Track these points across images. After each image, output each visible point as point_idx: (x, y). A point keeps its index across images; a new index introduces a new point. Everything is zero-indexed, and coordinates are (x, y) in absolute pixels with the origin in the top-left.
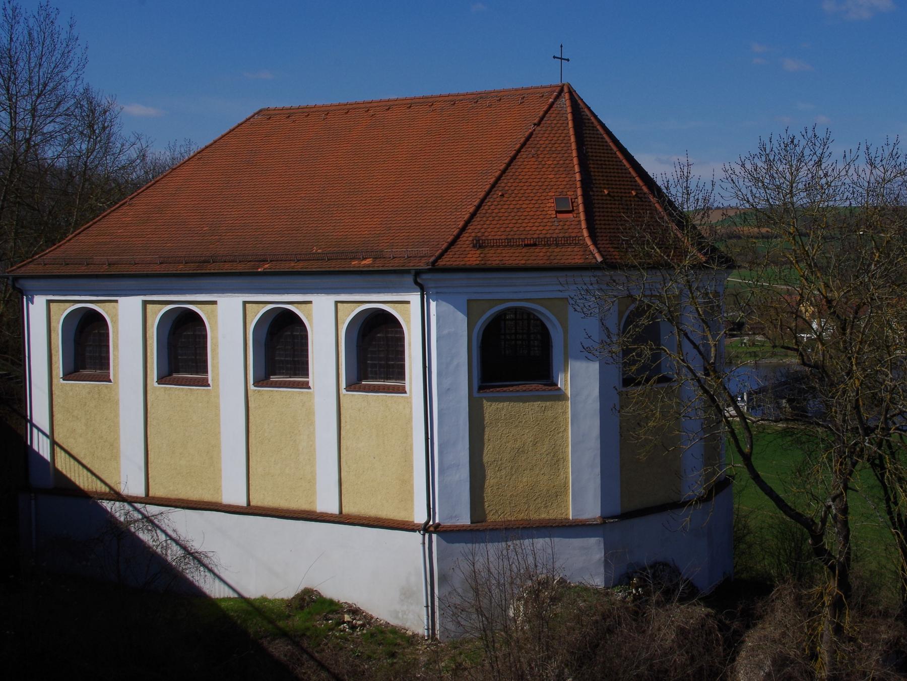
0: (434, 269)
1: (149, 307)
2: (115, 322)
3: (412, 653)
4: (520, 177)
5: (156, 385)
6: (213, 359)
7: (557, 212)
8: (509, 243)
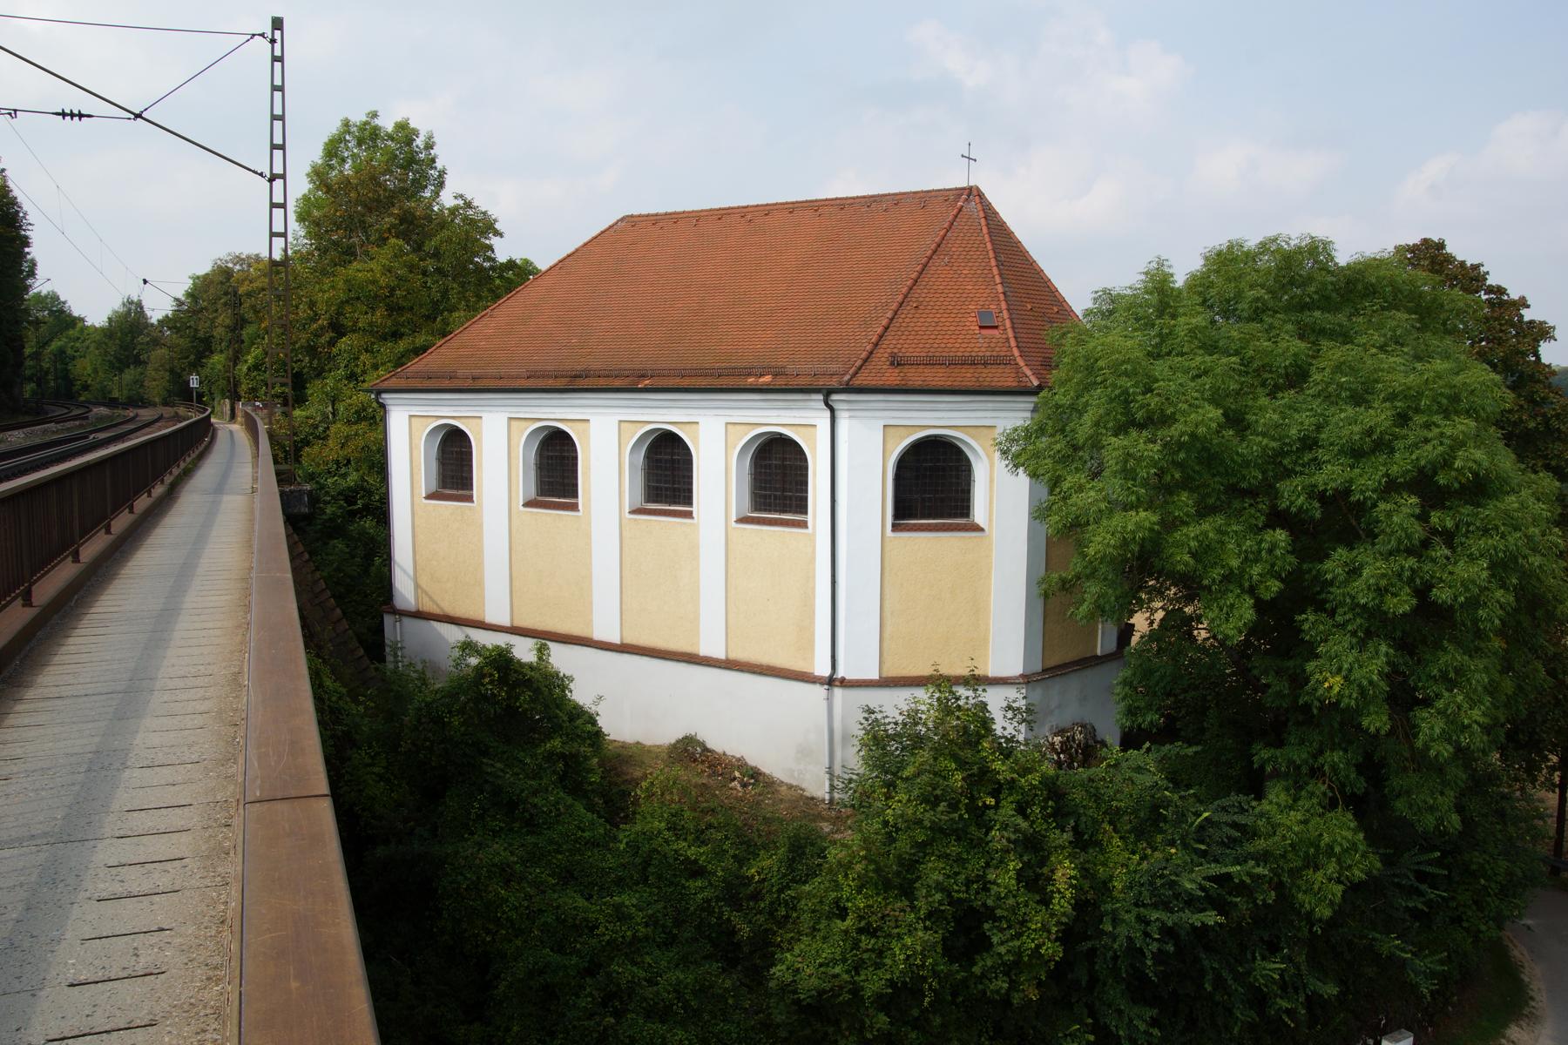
0: (849, 389)
1: (514, 423)
2: (480, 441)
3: (1549, 779)
8: (931, 362)
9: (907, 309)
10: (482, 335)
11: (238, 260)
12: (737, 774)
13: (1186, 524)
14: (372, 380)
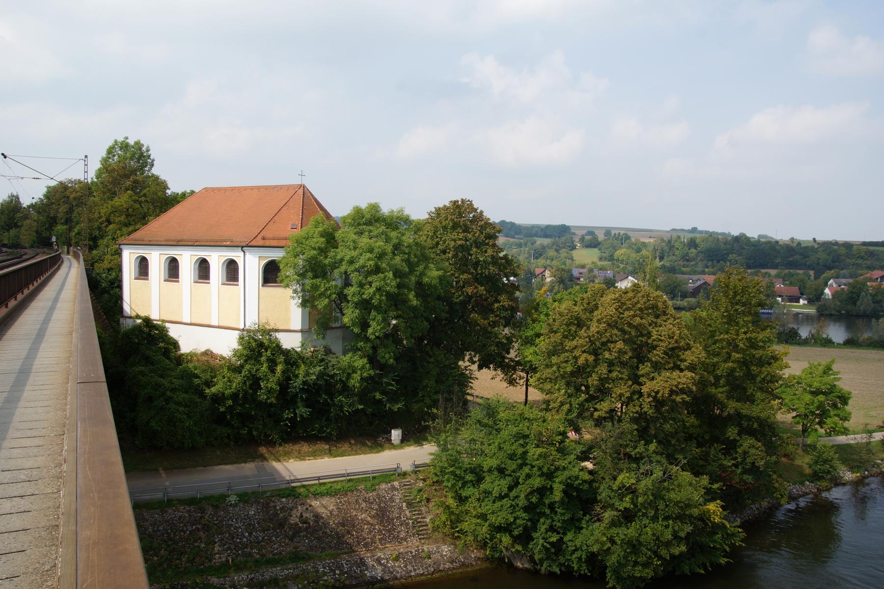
0: (247, 246)
10: (158, 226)
11: (71, 181)
14: (120, 241)
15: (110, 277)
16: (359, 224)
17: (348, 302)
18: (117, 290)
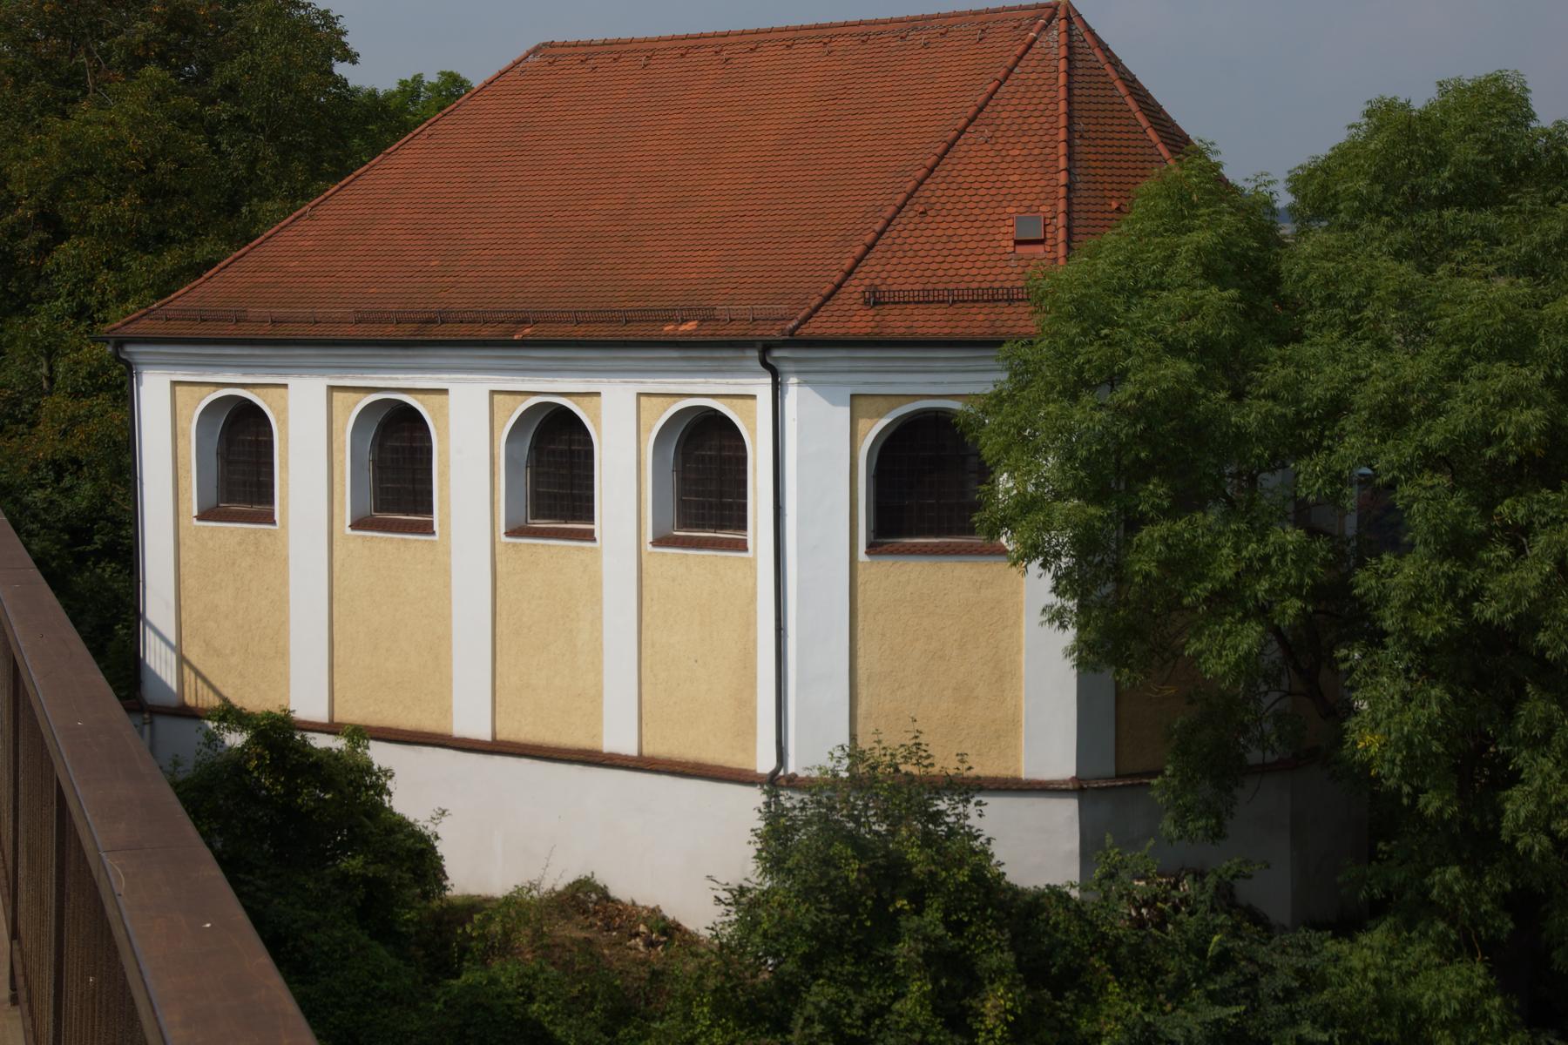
0: (794, 342)
1: (337, 396)
2: (284, 423)
4: (960, 179)
5: (348, 531)
6: (441, 490)
7: (1018, 242)
8: (927, 299)
9: (909, 214)
10: (304, 245)
12: (642, 928)
13: (1153, 522)
14: (116, 323)
15: (67, 506)
16: (1415, 202)
17: (1376, 638)
18: (108, 569)
